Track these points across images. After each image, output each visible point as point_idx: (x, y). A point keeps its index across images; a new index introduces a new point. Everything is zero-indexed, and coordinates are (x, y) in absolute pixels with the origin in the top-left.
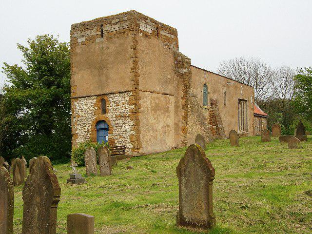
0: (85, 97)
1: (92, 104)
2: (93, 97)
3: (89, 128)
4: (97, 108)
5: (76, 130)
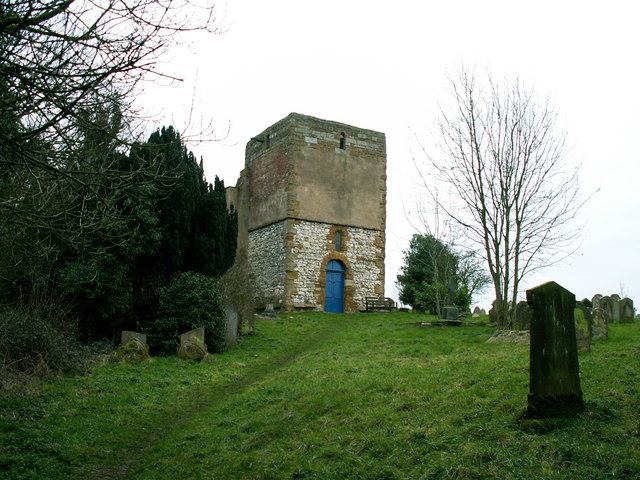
0: (314, 222)
2: (326, 226)
5: (296, 266)
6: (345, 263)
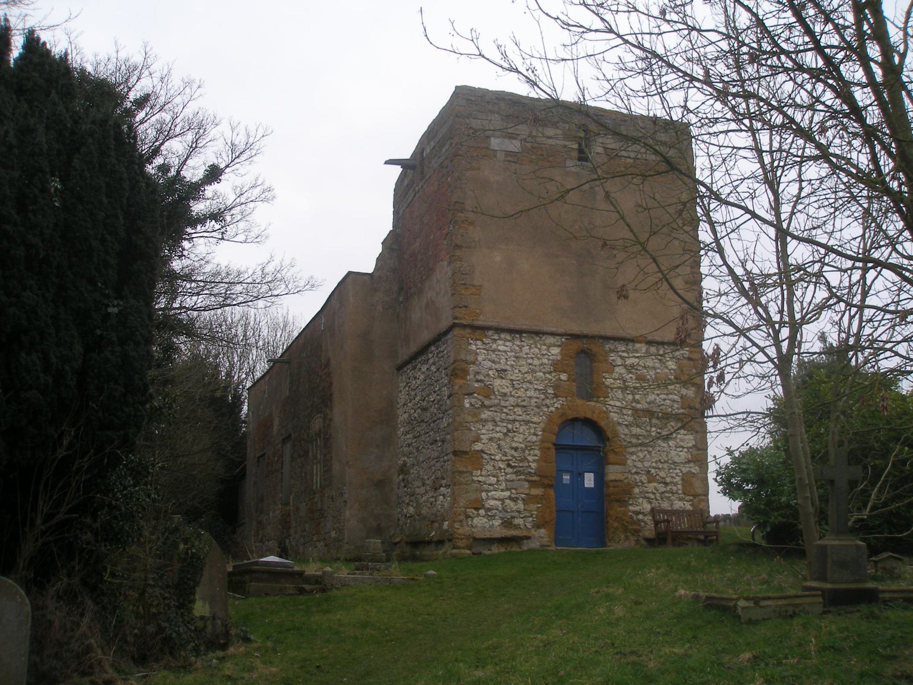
0: (520, 332)
1: (545, 361)
2: (551, 340)
3: (534, 439)
4: (564, 377)
5: (478, 439)
6: (602, 424)
